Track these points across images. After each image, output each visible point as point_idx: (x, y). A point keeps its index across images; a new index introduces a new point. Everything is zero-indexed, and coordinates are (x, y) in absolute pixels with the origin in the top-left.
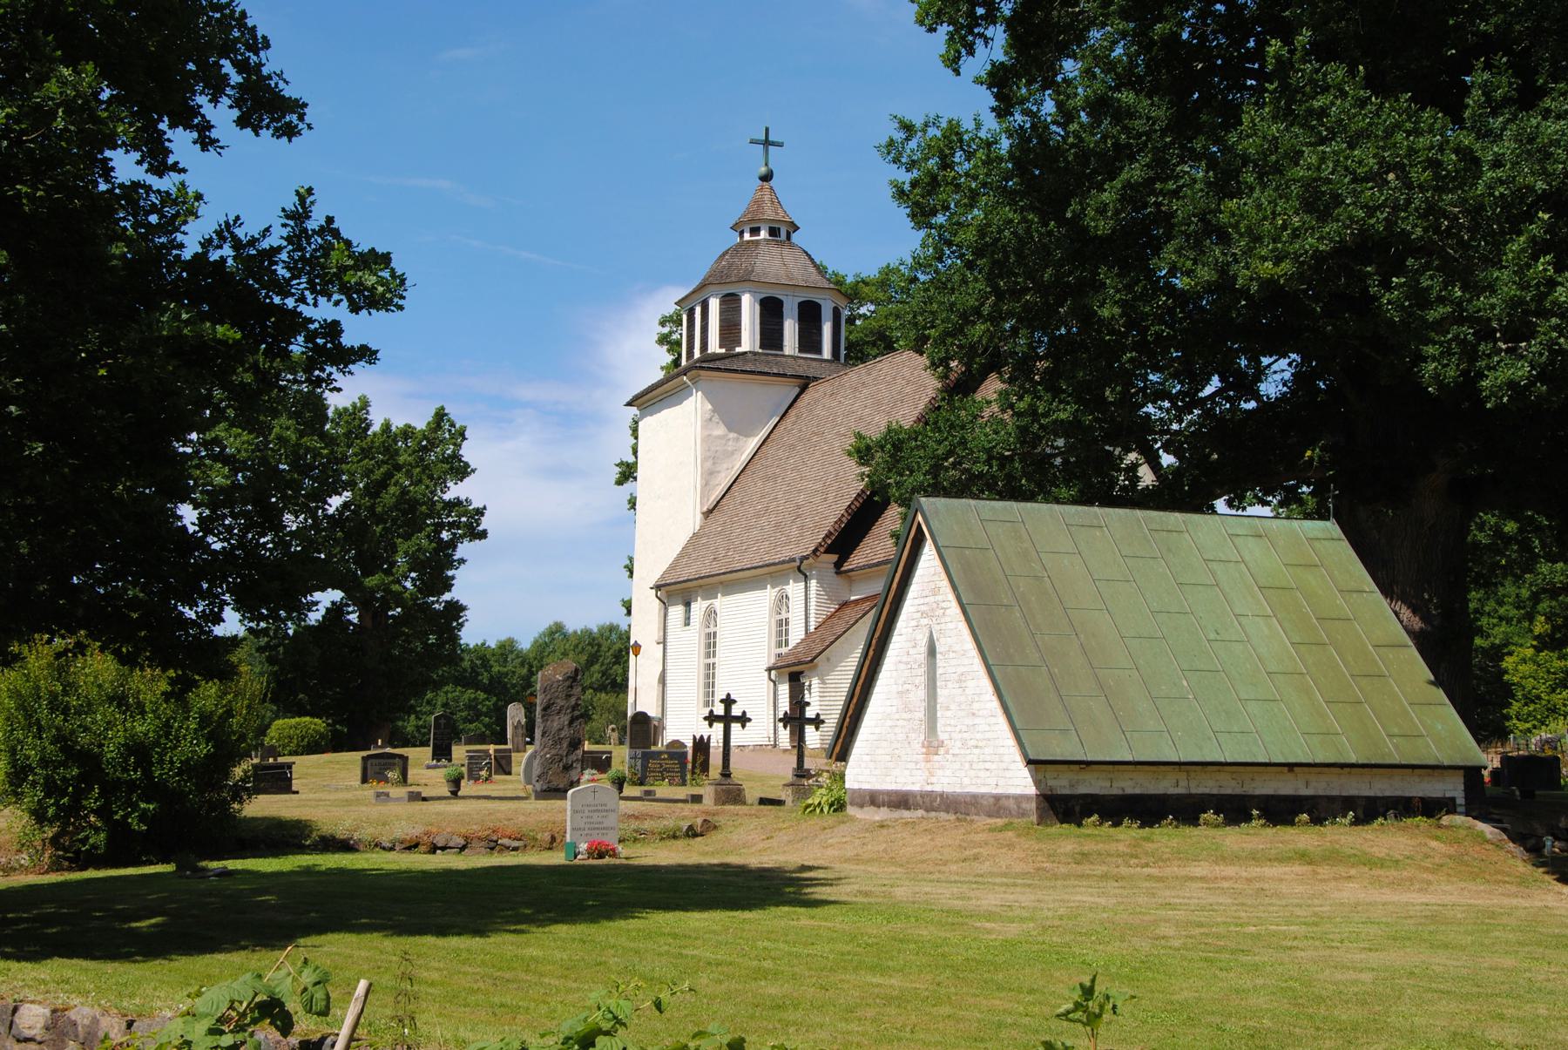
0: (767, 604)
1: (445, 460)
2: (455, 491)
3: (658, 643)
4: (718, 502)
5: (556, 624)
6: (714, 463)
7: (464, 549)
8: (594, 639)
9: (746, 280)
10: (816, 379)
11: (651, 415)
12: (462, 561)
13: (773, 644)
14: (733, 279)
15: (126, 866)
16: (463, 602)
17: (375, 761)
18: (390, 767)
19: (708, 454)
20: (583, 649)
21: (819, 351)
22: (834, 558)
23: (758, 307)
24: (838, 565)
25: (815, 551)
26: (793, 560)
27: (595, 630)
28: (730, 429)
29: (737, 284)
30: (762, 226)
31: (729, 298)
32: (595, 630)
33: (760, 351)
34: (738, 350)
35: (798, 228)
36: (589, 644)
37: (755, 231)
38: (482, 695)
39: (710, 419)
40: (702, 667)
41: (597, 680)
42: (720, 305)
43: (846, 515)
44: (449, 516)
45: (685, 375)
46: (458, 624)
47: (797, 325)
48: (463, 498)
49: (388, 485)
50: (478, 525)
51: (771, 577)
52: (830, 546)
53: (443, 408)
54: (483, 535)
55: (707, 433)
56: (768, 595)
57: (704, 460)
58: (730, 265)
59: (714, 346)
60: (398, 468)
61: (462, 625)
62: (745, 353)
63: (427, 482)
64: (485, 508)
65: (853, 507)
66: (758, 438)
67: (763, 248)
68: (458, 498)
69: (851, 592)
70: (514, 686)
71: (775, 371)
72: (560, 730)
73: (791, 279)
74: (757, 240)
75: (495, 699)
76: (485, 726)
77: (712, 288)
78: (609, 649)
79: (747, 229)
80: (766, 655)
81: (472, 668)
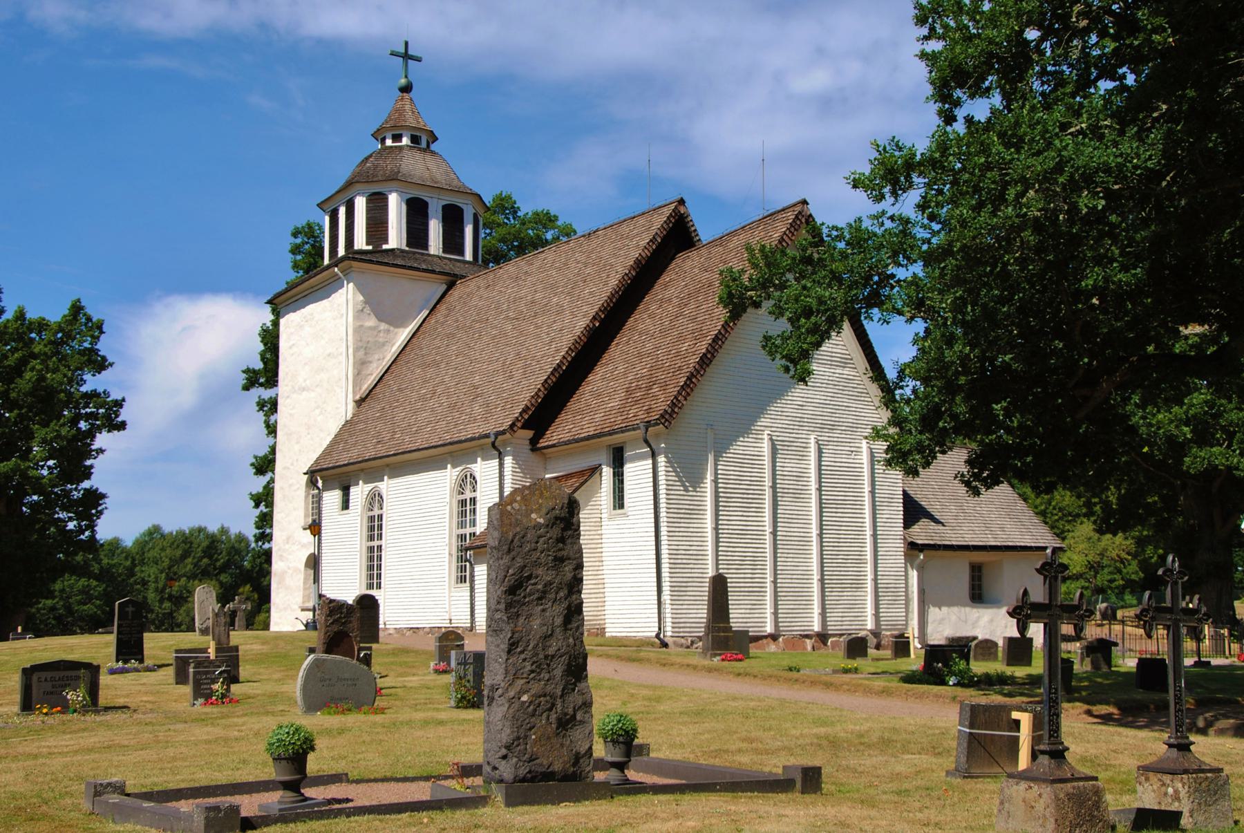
0: (448, 484)
1: (83, 353)
2: (92, 382)
3: (305, 529)
4: (371, 391)
5: (154, 526)
6: (366, 354)
7: (102, 440)
8: (186, 538)
9: (394, 178)
10: (463, 277)
11: (294, 311)
12: (100, 451)
13: (455, 525)
14: (380, 178)
15: (417, 248)
16: (102, 490)
17: (43, 675)
18: (72, 684)
19: (360, 344)
20: (178, 546)
21: (462, 253)
22: (529, 434)
23: (404, 207)
24: (534, 442)
25: (512, 426)
26: (487, 436)
27: (187, 532)
28: (380, 320)
29: (385, 183)
30: (404, 132)
31: (376, 197)
32: (187, 532)
33: (407, 249)
34: (385, 247)
35: (437, 139)
36: (183, 542)
37: (397, 138)
38: (94, 583)
39: (362, 310)
40: (364, 550)
41: (190, 570)
42: (367, 203)
43: (542, 389)
44: (86, 406)
45: (336, 266)
46: (97, 512)
47: (441, 225)
48: (100, 390)
49: (23, 372)
50: (117, 416)
51: (451, 456)
52: (526, 421)
53: (79, 300)
54: (122, 426)
55: (358, 324)
56: (448, 476)
57: (356, 350)
58: (376, 167)
59: (360, 242)
60: (34, 356)
61: (101, 512)
62: (393, 250)
63: (65, 370)
64: (123, 400)
65: (550, 381)
66: (411, 327)
67: (405, 152)
68: (95, 390)
69: (546, 471)
70: (120, 575)
71: (424, 267)
72: (547, 637)
73: (436, 183)
74: (399, 146)
75: (104, 585)
76: (96, 607)
77: (358, 187)
78: (199, 546)
79: (389, 135)
80: (447, 536)
81: (85, 561)
